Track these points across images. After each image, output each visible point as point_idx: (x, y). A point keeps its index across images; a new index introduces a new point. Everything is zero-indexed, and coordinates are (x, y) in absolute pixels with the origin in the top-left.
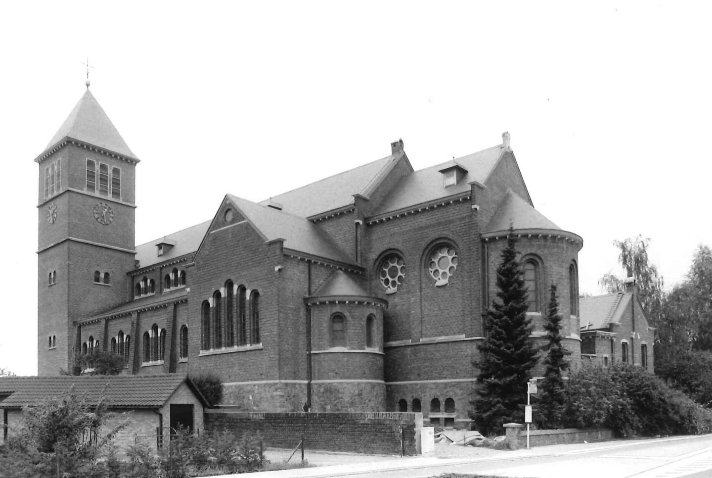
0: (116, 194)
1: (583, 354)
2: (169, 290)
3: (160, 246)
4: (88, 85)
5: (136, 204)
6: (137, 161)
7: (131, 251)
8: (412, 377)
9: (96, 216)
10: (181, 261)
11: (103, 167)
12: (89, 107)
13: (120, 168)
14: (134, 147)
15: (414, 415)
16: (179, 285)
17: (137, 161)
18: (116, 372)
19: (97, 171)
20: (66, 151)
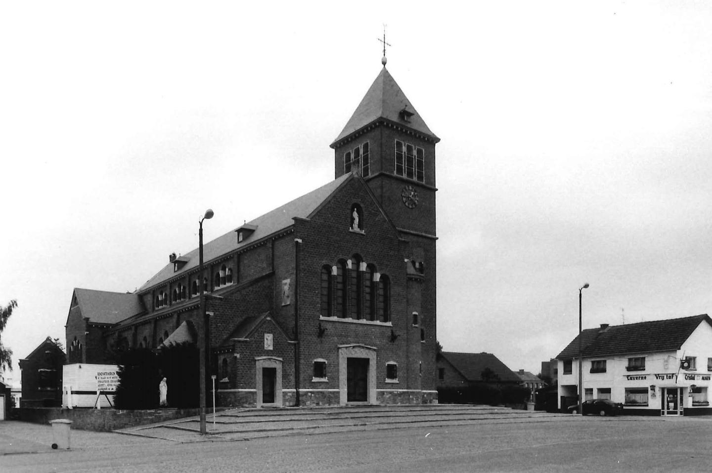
0: (420, 177)
1: (376, 318)
2: (195, 296)
3: (239, 231)
4: (384, 63)
5: (436, 187)
6: (438, 140)
7: (430, 236)
8: (290, 394)
9: (404, 199)
10: (258, 246)
11: (409, 149)
12: (386, 85)
13: (413, 145)
14: (434, 126)
15: (564, 387)
16: (227, 283)
17: (438, 140)
18: (482, 375)
19: (405, 153)
20: (377, 133)
